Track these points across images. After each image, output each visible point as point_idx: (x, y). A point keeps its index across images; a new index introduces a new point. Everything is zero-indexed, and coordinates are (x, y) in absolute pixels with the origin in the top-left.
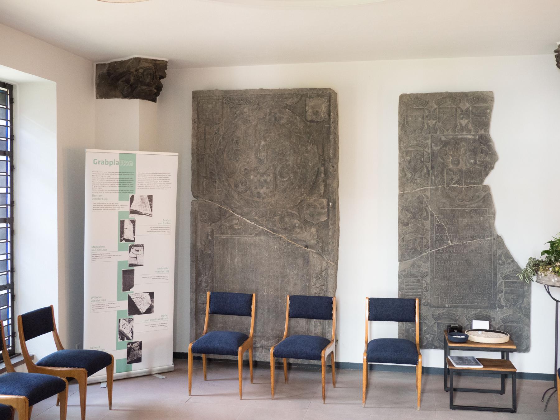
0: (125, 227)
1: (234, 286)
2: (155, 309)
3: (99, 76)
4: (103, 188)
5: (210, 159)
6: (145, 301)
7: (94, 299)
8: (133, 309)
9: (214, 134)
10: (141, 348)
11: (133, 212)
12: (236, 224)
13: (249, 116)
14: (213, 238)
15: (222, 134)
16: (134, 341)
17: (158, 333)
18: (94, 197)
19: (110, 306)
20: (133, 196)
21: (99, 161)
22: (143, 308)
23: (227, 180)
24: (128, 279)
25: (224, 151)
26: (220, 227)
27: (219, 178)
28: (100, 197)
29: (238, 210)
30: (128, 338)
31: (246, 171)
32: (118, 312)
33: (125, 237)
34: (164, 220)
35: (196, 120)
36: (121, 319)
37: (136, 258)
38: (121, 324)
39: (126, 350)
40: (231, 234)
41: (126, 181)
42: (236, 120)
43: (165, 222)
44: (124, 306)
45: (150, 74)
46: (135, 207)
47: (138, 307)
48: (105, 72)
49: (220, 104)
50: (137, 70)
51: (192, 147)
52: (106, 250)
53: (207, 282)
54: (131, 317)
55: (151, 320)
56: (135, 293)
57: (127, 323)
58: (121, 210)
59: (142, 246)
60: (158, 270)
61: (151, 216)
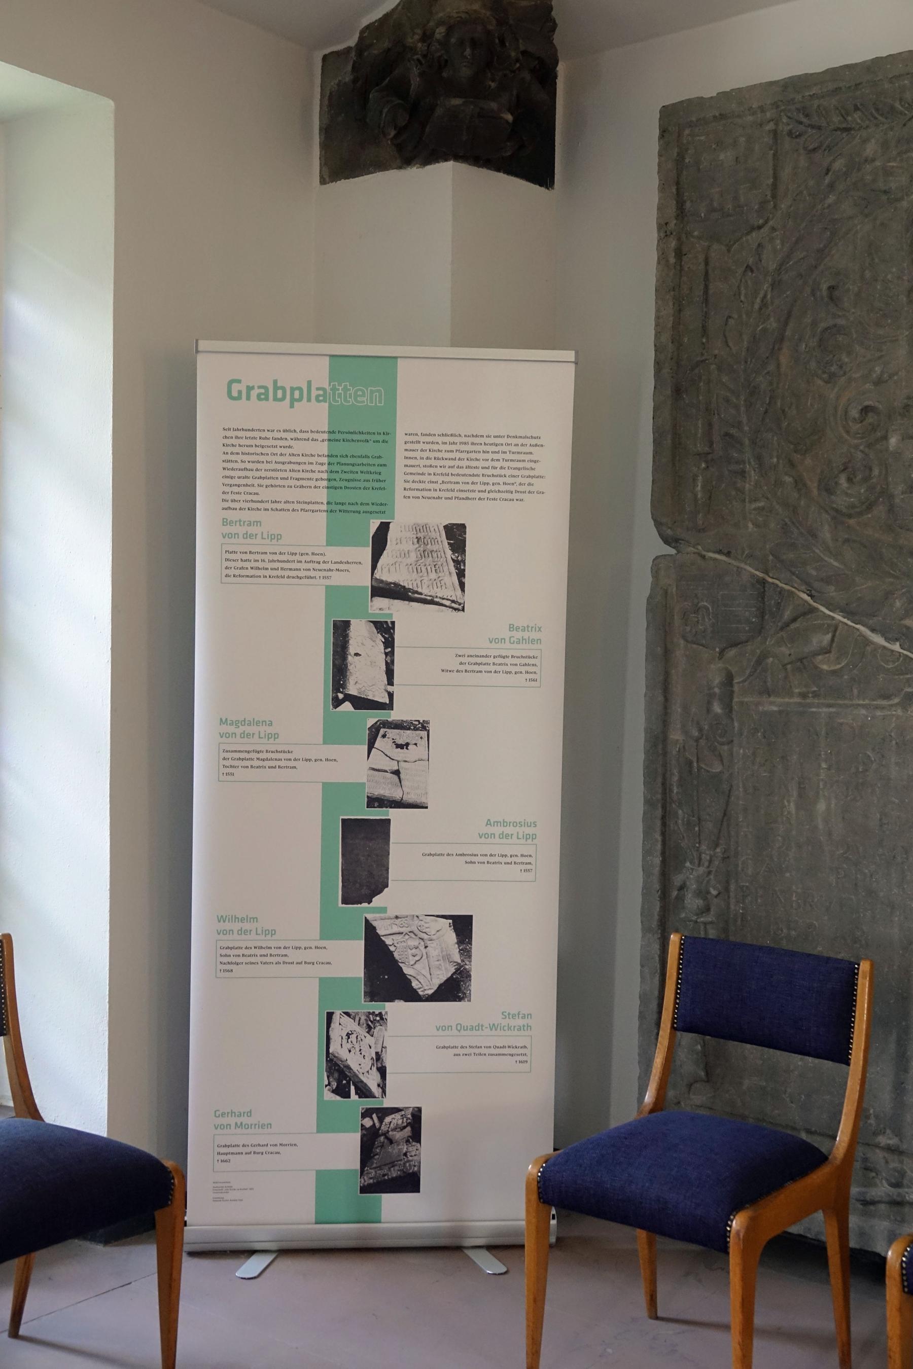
0: (352, 649)
1: (805, 915)
2: (476, 985)
3: (330, 98)
4: (266, 494)
5: (725, 379)
6: (434, 951)
7: (228, 926)
8: (385, 977)
9: (740, 270)
10: (416, 1136)
11: (382, 590)
12: (827, 651)
13: (888, 173)
14: (728, 708)
15: (772, 266)
16: (387, 1103)
17: (488, 1081)
18: (228, 529)
19: (294, 956)
20: (384, 528)
21: (250, 389)
22: (426, 974)
23: (792, 464)
24: (362, 855)
25: (781, 339)
26: (759, 662)
27: (759, 458)
28: (252, 530)
29: (831, 591)
30: (364, 1092)
31: (871, 418)
32: (326, 984)
33: (352, 690)
34: (512, 627)
35: (672, 225)
36: (338, 1013)
37: (397, 773)
38: (337, 1032)
39: (355, 1139)
40: (804, 696)
41: (358, 467)
42: (832, 199)
43: (519, 635)
44: (351, 959)
45: (474, 43)
46: (390, 570)
47: (406, 970)
48: (348, 78)
49: (768, 140)
50: (426, 37)
51: (658, 335)
52: (276, 736)
53: (702, 893)
54: (376, 1007)
55: (460, 1027)
56: (391, 913)
57: (362, 1031)
58: (338, 579)
59: (423, 726)
60: (491, 830)
61: (459, 607)
